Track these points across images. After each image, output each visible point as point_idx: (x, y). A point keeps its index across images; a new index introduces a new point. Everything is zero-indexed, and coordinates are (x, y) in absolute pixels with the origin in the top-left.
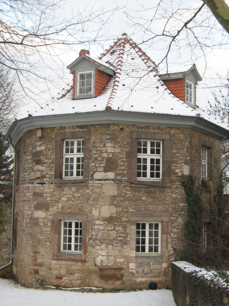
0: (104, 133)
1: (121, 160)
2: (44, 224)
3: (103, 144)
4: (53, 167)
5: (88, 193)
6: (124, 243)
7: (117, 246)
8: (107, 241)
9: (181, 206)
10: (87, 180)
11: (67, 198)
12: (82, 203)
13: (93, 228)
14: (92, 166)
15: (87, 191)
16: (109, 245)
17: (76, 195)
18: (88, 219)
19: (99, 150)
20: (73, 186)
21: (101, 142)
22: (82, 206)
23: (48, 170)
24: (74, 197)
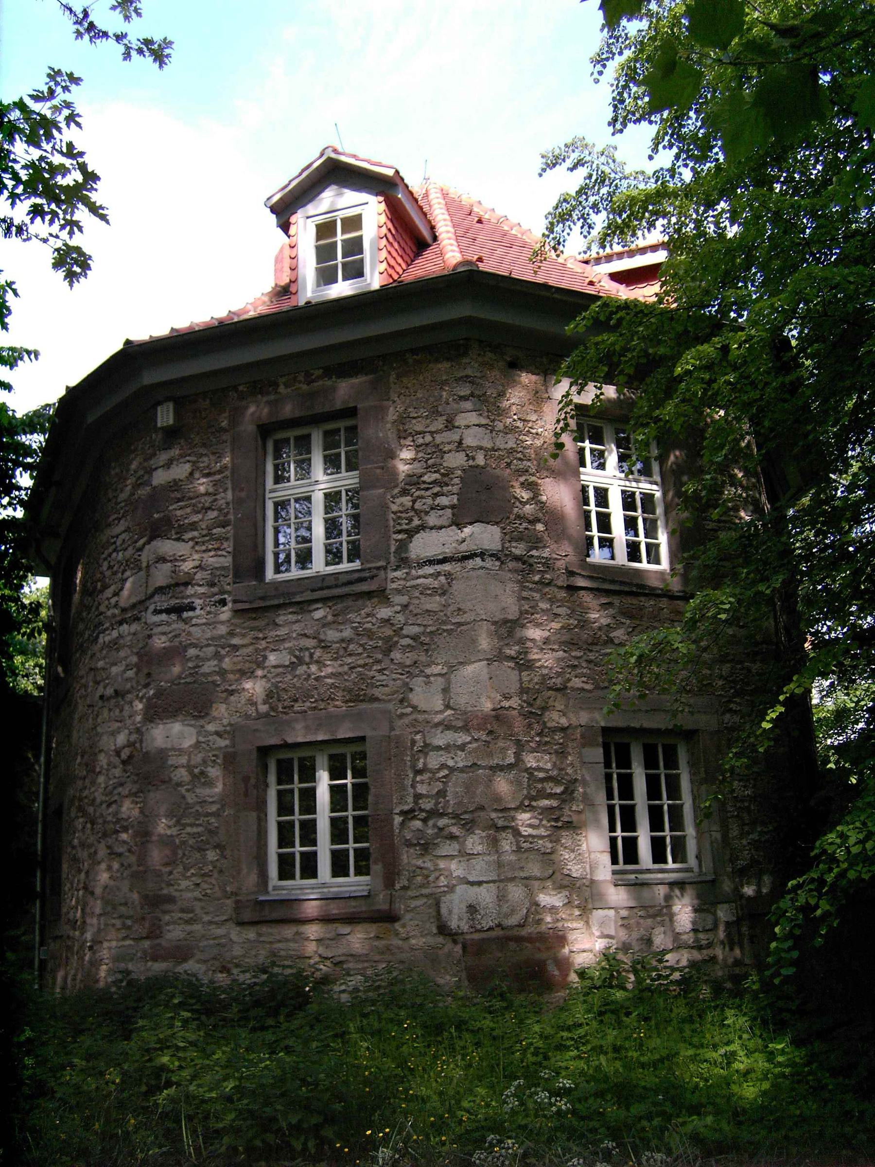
0: (444, 378)
1: (522, 479)
2: (191, 772)
3: (444, 418)
4: (227, 539)
5: (387, 621)
6: (560, 824)
7: (533, 837)
8: (494, 815)
9: (754, 671)
10: (378, 568)
11: (291, 652)
12: (360, 666)
13: (420, 765)
14: (401, 512)
15: (384, 612)
16: (504, 835)
17: (331, 635)
18: (392, 729)
19: (427, 445)
20: (316, 601)
21: (435, 413)
22: (362, 677)
23: (204, 551)
24: (325, 646)
